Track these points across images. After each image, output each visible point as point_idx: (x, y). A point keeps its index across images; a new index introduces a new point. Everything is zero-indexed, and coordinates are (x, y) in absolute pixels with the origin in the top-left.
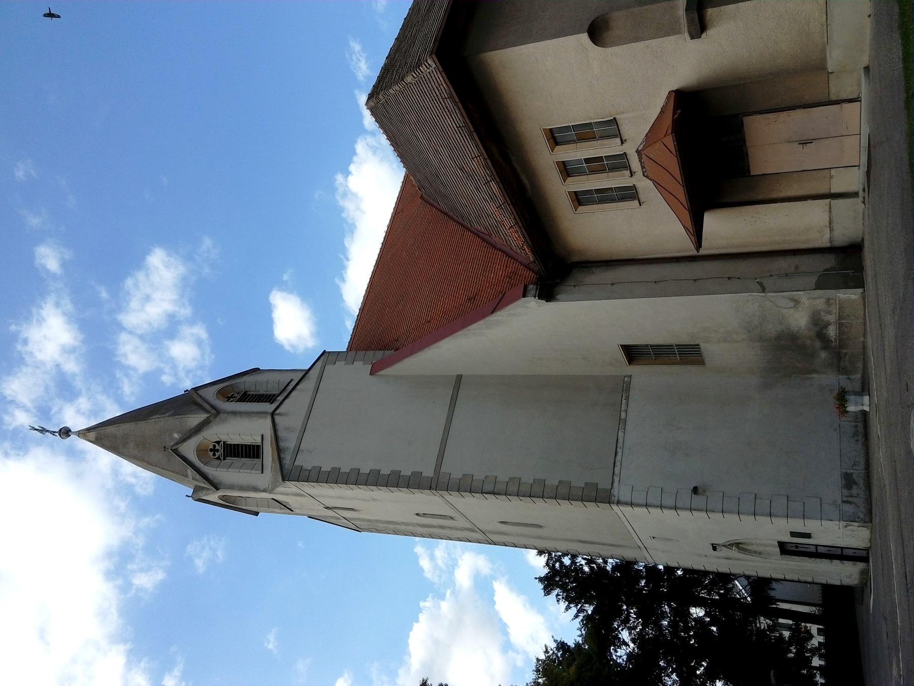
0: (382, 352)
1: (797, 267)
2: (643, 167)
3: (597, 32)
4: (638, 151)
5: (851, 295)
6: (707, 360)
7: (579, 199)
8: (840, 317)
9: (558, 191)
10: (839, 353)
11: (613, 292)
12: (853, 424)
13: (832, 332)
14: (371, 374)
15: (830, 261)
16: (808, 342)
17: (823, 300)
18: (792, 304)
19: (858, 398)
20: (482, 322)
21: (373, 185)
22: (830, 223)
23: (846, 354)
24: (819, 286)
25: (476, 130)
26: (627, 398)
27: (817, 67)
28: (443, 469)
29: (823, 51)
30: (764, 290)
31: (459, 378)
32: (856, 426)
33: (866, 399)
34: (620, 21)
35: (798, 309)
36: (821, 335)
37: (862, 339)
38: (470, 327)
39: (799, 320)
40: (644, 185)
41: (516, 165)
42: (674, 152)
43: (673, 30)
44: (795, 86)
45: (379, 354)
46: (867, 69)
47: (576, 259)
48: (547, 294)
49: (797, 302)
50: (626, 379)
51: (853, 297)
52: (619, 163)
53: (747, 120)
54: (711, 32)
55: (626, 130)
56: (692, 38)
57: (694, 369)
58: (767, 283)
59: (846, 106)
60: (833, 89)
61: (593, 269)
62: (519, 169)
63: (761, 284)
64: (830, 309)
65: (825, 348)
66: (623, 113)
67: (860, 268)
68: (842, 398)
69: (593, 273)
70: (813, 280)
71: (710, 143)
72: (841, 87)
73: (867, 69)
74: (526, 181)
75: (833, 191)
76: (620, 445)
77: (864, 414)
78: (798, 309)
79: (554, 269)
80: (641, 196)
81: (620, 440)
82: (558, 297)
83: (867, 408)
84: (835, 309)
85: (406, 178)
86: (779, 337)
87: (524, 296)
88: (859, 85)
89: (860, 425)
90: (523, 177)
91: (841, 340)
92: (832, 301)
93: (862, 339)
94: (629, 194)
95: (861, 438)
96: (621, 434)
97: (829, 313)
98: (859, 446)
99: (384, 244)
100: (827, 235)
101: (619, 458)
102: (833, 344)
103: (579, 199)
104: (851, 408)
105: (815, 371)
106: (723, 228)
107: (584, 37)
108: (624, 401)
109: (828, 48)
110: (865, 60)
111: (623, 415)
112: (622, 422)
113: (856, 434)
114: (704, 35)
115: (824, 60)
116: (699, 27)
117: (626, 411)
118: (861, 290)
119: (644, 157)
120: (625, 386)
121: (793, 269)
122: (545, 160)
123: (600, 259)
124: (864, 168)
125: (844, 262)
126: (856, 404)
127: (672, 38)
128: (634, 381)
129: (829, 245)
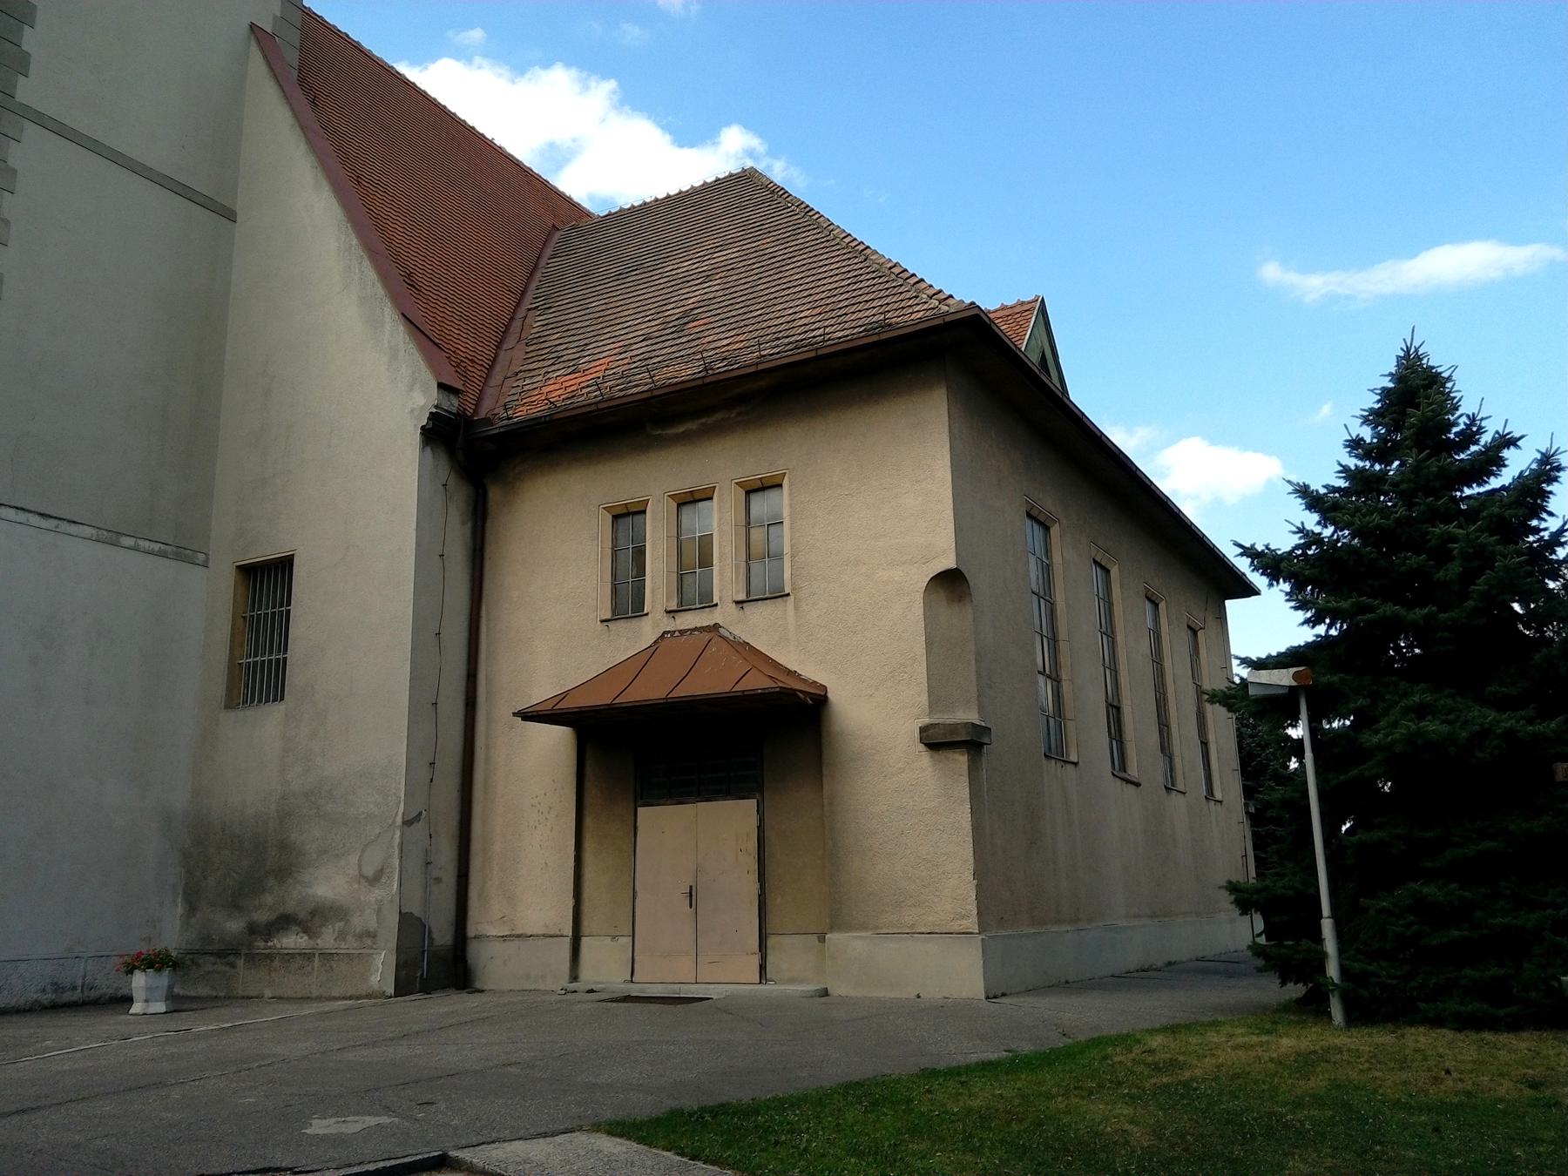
0: (296, 64)
1: (438, 880)
2: (682, 632)
3: (950, 583)
4: (716, 627)
5: (381, 971)
6: (232, 714)
7: (627, 516)
8: (327, 956)
9: (650, 479)
10: (237, 954)
11: (428, 555)
12: (79, 983)
13: (292, 941)
14: (253, 27)
15: (442, 935)
16: (269, 899)
17: (373, 925)
18: (369, 871)
19: (162, 992)
20: (380, 290)
21: (599, 147)
22: (519, 936)
23: (233, 965)
24: (405, 919)
25: (817, 358)
26: (162, 554)
27: (836, 913)
28: (30, 129)
29: (863, 927)
30: (407, 823)
31: (230, 215)
32: (74, 988)
33: (160, 1007)
34: (958, 619)
35: (358, 885)
36: (285, 922)
37: (268, 993)
38: (367, 263)
39: (327, 884)
40: (645, 632)
41: (718, 416)
42: (739, 688)
43: (935, 702)
44: (803, 884)
45: (293, 57)
46: (825, 993)
47: (494, 494)
48: (441, 433)
49: (374, 880)
50: (201, 556)
51: (375, 979)
52: (692, 591)
53: (751, 804)
54: (925, 758)
55: (760, 615)
56: (923, 730)
57: (219, 690)
58: (419, 829)
59: (755, 961)
60: (787, 940)
61: (469, 525)
62: (709, 420)
63: (417, 818)
64: (349, 938)
65: (253, 929)
66: (796, 608)
67: (428, 987)
68: (154, 962)
69: (463, 523)
70: (416, 909)
71: (709, 742)
72: (791, 955)
73: (825, 993)
74: (681, 429)
75: (584, 941)
76: (64, 526)
77: (128, 1000)
78: (358, 885)
79: (479, 455)
80: (620, 626)
81: (73, 529)
82: (428, 449)
83: (137, 1008)
84: (349, 946)
85: (588, 214)
86: (284, 846)
87: (441, 386)
88: (792, 981)
89: (76, 996)
90: (692, 425)
91: (270, 957)
92: (369, 942)
93: (268, 993)
94: (627, 602)
95: (49, 997)
96: (88, 531)
97: (341, 936)
98: (33, 996)
99: (472, 131)
100: (493, 931)
101: (34, 520)
102: (261, 944)
103: (627, 516)
104: (139, 980)
105: (192, 909)
106: (533, 770)
107: (949, 563)
108: (156, 547)
109: (869, 934)
110: (838, 990)
111: (129, 542)
112: (112, 537)
113: (58, 987)
114: (922, 747)
115: (847, 927)
116: (936, 741)
117: (136, 549)
118: (391, 990)
119: (707, 636)
120: (185, 552)
121: (436, 873)
122: (723, 463)
123: (489, 537)
124: (635, 990)
125: (441, 963)
126: (149, 989)
127: (924, 698)
128: (199, 572)
129: (471, 932)
